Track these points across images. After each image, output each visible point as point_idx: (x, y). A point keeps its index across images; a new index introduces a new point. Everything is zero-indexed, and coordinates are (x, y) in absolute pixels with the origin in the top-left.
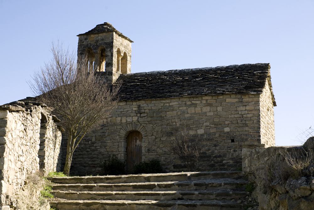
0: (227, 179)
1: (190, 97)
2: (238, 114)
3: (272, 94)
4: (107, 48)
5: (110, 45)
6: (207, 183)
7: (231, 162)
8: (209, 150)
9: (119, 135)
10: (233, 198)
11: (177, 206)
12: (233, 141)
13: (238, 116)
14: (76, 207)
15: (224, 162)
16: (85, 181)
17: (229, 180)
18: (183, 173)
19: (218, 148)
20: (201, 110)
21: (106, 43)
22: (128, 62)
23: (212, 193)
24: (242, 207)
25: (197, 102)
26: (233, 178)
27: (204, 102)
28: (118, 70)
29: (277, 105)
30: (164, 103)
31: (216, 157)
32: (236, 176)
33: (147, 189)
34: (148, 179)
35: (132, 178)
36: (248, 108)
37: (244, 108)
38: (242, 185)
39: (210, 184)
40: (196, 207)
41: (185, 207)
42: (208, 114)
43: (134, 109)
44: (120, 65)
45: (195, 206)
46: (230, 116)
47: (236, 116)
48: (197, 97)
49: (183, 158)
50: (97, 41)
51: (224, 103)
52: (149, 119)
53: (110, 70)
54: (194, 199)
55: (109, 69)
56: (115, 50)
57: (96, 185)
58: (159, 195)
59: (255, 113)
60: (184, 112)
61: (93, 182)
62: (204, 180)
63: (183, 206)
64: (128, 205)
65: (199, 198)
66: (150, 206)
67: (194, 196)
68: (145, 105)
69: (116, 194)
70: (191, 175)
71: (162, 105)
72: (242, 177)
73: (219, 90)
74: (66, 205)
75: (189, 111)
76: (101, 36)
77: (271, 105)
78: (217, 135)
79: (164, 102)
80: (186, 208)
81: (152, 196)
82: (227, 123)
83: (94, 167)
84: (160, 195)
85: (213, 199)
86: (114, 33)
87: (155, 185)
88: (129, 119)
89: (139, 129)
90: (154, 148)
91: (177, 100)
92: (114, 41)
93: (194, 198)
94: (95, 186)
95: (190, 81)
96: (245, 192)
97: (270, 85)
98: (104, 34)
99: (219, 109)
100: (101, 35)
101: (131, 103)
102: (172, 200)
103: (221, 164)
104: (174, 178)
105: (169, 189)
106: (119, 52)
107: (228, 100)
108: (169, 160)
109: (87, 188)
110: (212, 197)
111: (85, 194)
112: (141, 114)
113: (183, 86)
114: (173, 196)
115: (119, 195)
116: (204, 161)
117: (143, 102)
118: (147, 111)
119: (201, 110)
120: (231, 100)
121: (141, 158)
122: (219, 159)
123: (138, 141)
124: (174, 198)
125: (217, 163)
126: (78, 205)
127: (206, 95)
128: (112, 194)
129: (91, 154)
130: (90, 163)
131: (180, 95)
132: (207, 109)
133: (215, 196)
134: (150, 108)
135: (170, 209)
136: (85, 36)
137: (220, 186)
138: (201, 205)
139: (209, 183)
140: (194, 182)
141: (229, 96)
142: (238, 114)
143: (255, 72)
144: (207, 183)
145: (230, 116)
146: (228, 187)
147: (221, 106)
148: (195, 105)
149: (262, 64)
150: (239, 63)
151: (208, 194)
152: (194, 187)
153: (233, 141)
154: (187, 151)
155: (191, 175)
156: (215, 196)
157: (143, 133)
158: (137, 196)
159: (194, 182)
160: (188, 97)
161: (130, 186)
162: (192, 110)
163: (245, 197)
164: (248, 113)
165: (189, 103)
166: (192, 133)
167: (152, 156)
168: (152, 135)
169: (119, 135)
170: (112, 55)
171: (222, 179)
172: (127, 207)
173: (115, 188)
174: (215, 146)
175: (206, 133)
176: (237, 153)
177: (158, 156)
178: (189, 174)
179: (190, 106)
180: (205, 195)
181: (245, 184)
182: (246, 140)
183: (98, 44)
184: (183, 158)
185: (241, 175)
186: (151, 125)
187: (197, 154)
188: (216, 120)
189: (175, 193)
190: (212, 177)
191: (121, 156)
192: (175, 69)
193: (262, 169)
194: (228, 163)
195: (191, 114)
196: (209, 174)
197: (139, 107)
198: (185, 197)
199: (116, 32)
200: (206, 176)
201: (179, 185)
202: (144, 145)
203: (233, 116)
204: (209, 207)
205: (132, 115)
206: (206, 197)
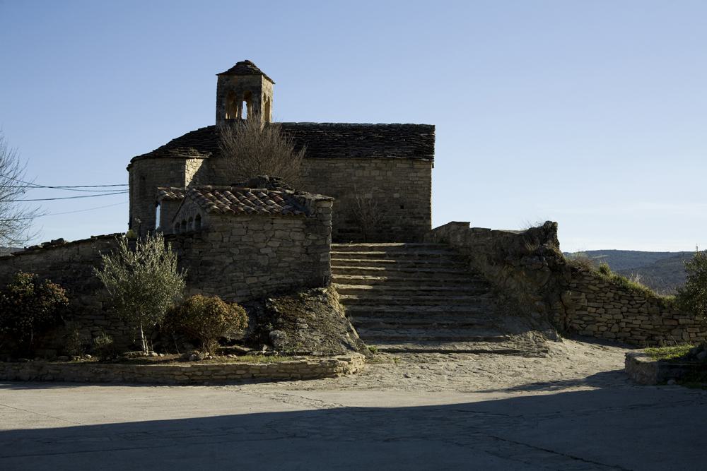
12: (402, 207)
13: (409, 182)
15: (393, 228)
19: (386, 214)
20: (370, 173)
21: (253, 88)
29: (536, 221)
31: (384, 223)
34: (372, 249)
36: (419, 174)
37: (415, 175)
42: (377, 178)
47: (406, 182)
50: (242, 84)
52: (312, 179)
71: (327, 165)
75: (357, 173)
76: (246, 78)
78: (386, 201)
82: (396, 188)
95: (354, 139)
98: (251, 76)
99: (389, 173)
100: (246, 76)
110: (439, 266)
113: (346, 145)
119: (370, 173)
120: (402, 165)
122: (387, 225)
128: (358, 262)
136: (227, 77)
143: (422, 135)
148: (364, 168)
149: (427, 125)
153: (402, 207)
162: (360, 173)
165: (357, 165)
173: (352, 256)
174: (384, 211)
182: (416, 207)
192: (331, 122)
193: (483, 245)
198: (417, 266)
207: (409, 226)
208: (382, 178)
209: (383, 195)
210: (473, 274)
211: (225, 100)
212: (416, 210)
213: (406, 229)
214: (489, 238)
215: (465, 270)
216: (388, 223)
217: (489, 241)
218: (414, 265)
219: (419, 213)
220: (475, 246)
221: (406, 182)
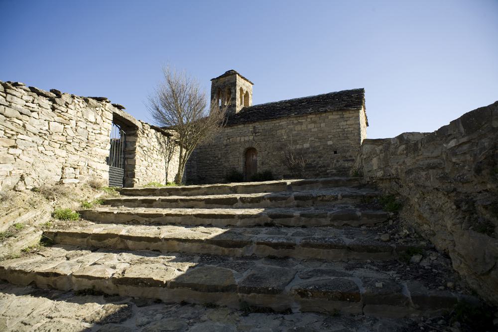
0: (344, 188)
1: (297, 117)
2: (340, 128)
3: (365, 114)
4: (232, 86)
5: (234, 84)
6: (315, 196)
7: (334, 171)
8: (314, 161)
9: (239, 152)
10: (362, 223)
11: (255, 246)
12: (335, 152)
13: (340, 130)
14: (82, 241)
15: (328, 171)
16: (158, 192)
17: (348, 191)
18: (283, 181)
21: (231, 83)
22: (250, 99)
23: (325, 215)
24: (394, 251)
25: (303, 121)
26: (351, 186)
27: (309, 120)
28: (241, 104)
30: (275, 123)
31: (320, 167)
32: (356, 184)
33: (225, 204)
35: (214, 189)
37: (345, 123)
38: (371, 197)
39: (320, 196)
40: (294, 249)
41: (271, 248)
42: (313, 130)
43: (251, 130)
44: (243, 100)
45: (292, 246)
46: (332, 131)
47: (338, 130)
48: (303, 116)
49: (291, 169)
50: (225, 82)
51: (327, 120)
52: (263, 137)
53: (234, 103)
54: (293, 225)
55: (233, 102)
56: (238, 89)
57: (157, 199)
58: (234, 218)
59: (356, 126)
60: (292, 130)
61: (168, 194)
62: (310, 191)
63: (267, 247)
64: (163, 241)
65: (302, 224)
66: (203, 244)
67: (292, 221)
68: (259, 126)
69: (167, 215)
70: (292, 183)
71: (273, 124)
72: (365, 185)
73: (321, 109)
74: (67, 237)
75: (296, 129)
77: (365, 125)
78: (321, 148)
79: (275, 122)
80: (274, 250)
81: (222, 218)
82: (329, 137)
83: (220, 178)
84: (235, 217)
85: (327, 226)
86: (237, 75)
87: (236, 198)
88: (247, 138)
89: (255, 146)
90: (267, 161)
91: (286, 120)
92: (237, 81)
93: (292, 223)
94: (155, 200)
96: (386, 213)
97: (365, 109)
98: (230, 76)
100: (227, 77)
101: (248, 125)
102: (255, 226)
103: (325, 173)
104: (269, 187)
105: (256, 204)
106: (241, 90)
107: (331, 117)
108: (279, 171)
109: (146, 203)
111: (124, 213)
112: (256, 133)
114: (257, 220)
115: (171, 217)
116: (310, 171)
117: (257, 123)
118: (261, 131)
121: (257, 170)
122: (323, 169)
123: (254, 156)
124: (256, 223)
125: (321, 172)
126: (85, 237)
127: (310, 114)
129: (218, 168)
130: (217, 175)
131: (289, 117)
132: (311, 126)
133: (331, 221)
134: (263, 128)
135: (241, 251)
137: (336, 200)
138: (306, 245)
139: (453, 262)
140: (295, 193)
141: (331, 113)
142: (340, 128)
144: (314, 195)
145: (332, 131)
146: (349, 202)
147: (324, 122)
148: (301, 123)
150: (338, 90)
151: (317, 216)
152: (294, 201)
153: (335, 152)
154: (293, 162)
155: (292, 183)
156: (330, 219)
157: (258, 149)
158: (198, 218)
159: (295, 193)
160: (295, 117)
161: (201, 200)
162: (298, 128)
163: (386, 221)
164: (349, 128)
165: (295, 122)
166: (298, 147)
167: (266, 168)
168: (266, 150)
169: (239, 152)
170: (236, 92)
171: (337, 189)
172: (163, 244)
173: (182, 204)
174: (320, 157)
175: (311, 146)
176: (339, 163)
177: (270, 168)
178: (289, 182)
179: (297, 124)
180: (312, 217)
181: (376, 196)
182: (348, 151)
183: (225, 85)
184: (291, 169)
185: (363, 182)
186: (265, 142)
187: (303, 164)
188: (320, 135)
189: (260, 214)
190: (321, 186)
191: (240, 169)
193: (430, 167)
194: (331, 172)
195: (298, 131)
196: (317, 182)
197: (254, 127)
199: (239, 75)
200: (312, 185)
201: (271, 199)
202: (259, 159)
203: (335, 131)
204: (321, 250)
205: (249, 134)
206: (313, 221)
207: (343, 168)
208: (317, 130)
209: (318, 144)
210: (411, 252)
211: (215, 95)
212: (348, 154)
213: (340, 171)
214: (452, 143)
215: (385, 237)
216: (324, 167)
217: (453, 151)
218: (270, 220)
219: (351, 156)
220: (409, 172)
221: (338, 130)
